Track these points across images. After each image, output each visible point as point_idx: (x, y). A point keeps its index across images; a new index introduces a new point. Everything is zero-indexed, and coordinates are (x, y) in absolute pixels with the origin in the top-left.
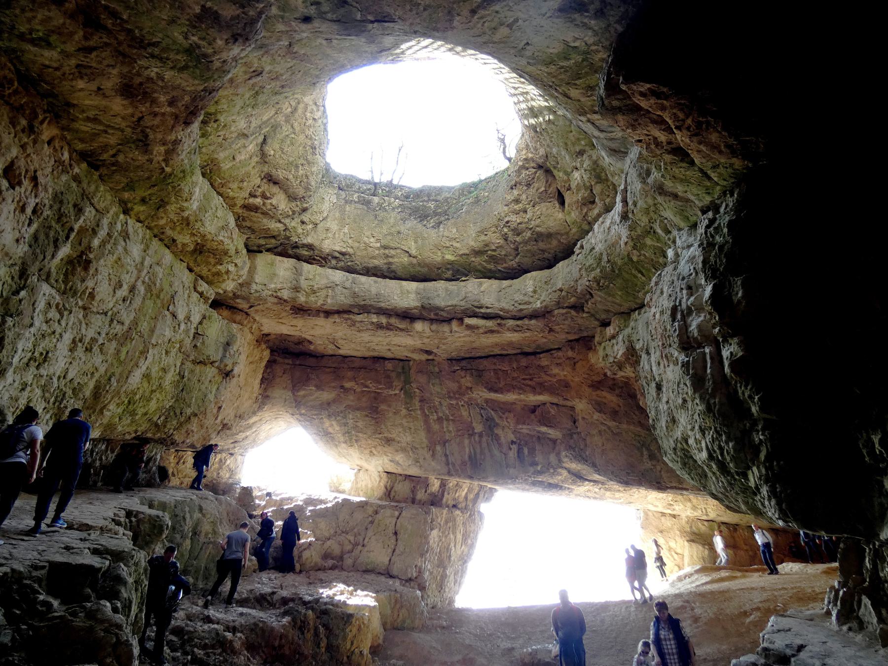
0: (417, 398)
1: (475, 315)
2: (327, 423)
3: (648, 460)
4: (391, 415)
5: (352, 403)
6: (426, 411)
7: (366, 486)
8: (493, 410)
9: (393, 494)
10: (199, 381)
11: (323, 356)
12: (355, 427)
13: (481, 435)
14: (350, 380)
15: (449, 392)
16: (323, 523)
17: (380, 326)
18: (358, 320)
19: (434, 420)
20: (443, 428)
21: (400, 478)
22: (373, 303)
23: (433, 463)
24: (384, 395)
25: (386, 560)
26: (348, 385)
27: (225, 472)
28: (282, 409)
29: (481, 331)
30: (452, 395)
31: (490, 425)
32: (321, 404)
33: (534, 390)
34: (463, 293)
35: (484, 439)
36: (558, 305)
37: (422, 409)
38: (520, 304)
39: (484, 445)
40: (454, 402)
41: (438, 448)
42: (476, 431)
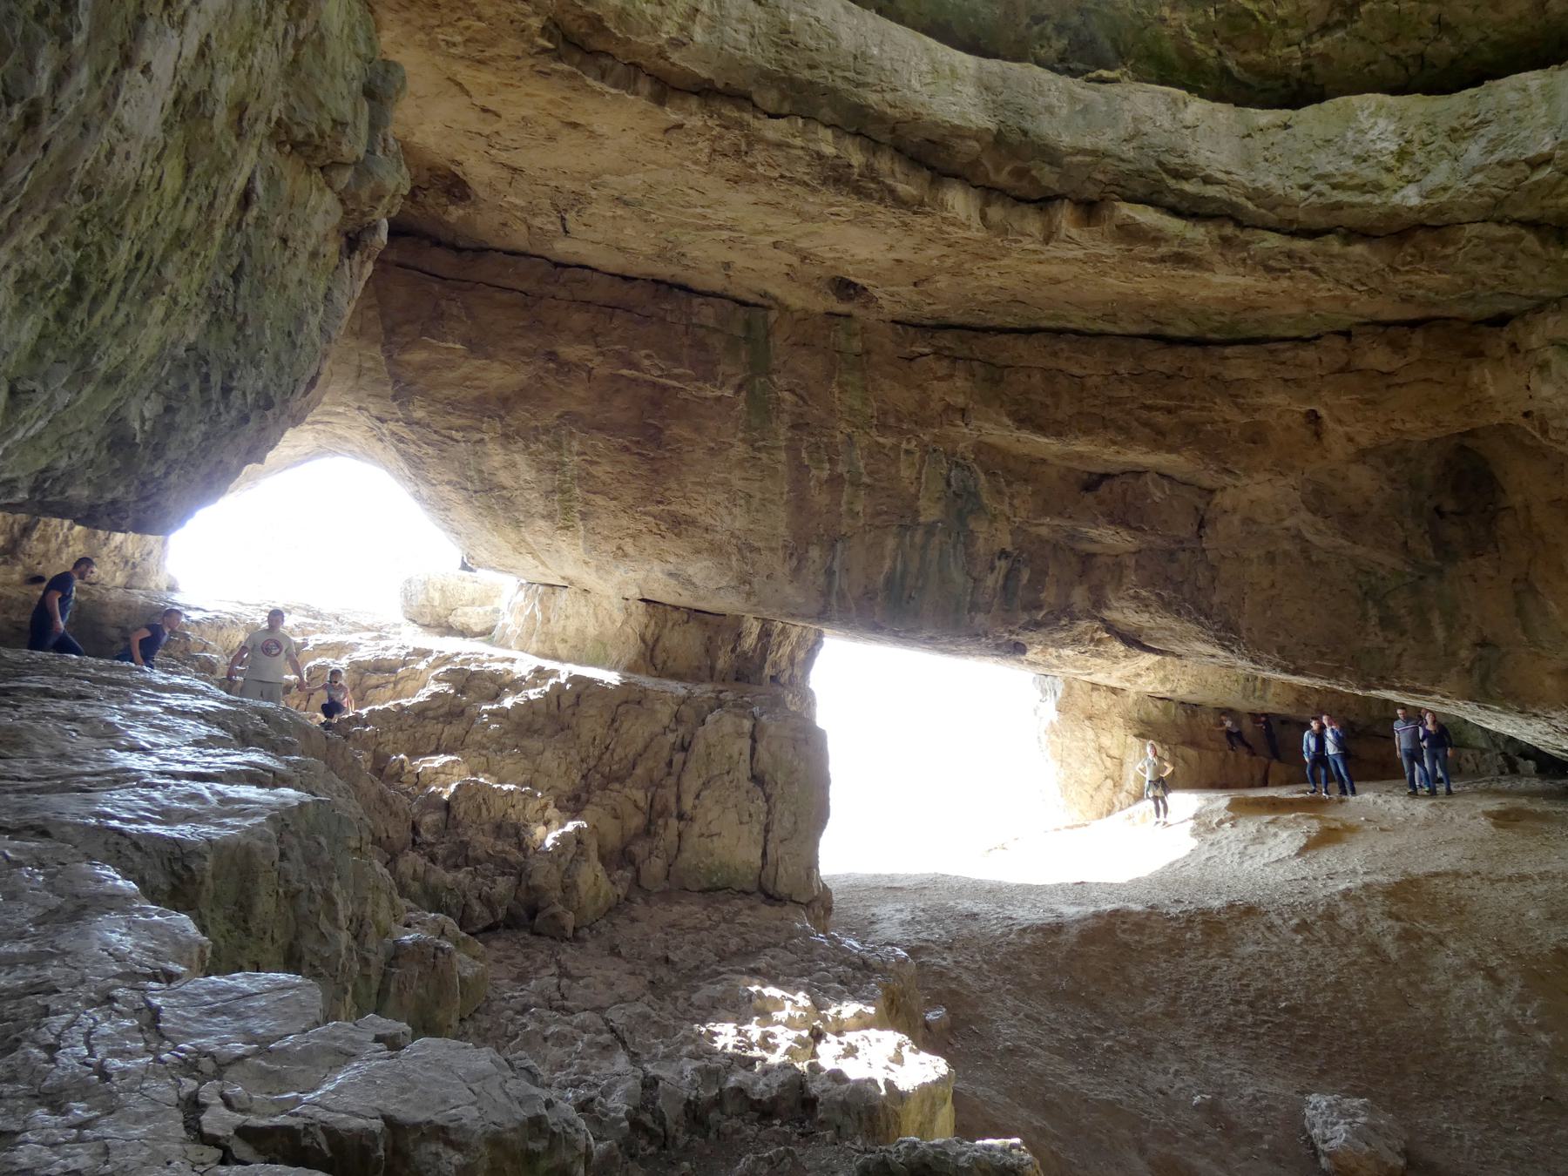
0: (786, 418)
1: (1150, 200)
2: (496, 457)
3: (1377, 630)
4: (699, 453)
5: (582, 409)
6: (804, 454)
7: (580, 632)
8: (986, 473)
9: (660, 656)
10: (284, 241)
11: (482, 251)
12: (584, 479)
13: (930, 530)
14: (579, 338)
15: (885, 413)
16: (548, 754)
17: (837, 177)
18: (770, 135)
19: (820, 484)
20: (839, 504)
21: (676, 615)
22: (840, 84)
23: (789, 590)
24: (682, 395)
25: (755, 856)
26: (572, 352)
27: (109, 567)
28: (348, 398)
29: (1163, 250)
30: (892, 421)
31: (963, 504)
32: (482, 401)
33: (1159, 439)
34: (1128, 116)
35: (936, 541)
36: (1495, 211)
37: (793, 449)
38: (1334, 187)
39: (933, 554)
40: (887, 441)
41: (815, 553)
42: (922, 519)
